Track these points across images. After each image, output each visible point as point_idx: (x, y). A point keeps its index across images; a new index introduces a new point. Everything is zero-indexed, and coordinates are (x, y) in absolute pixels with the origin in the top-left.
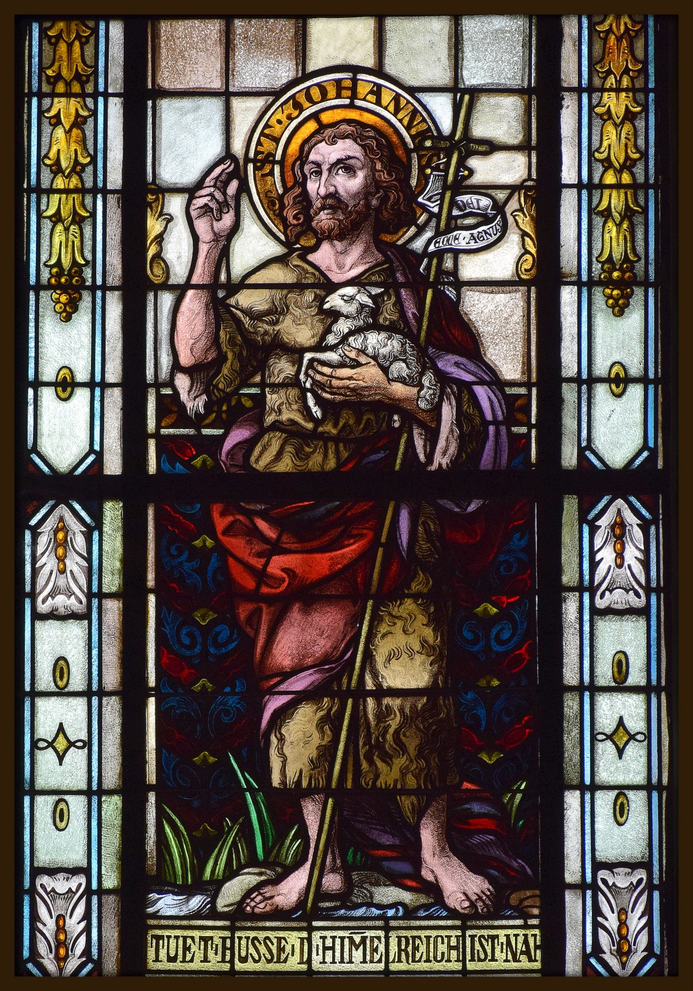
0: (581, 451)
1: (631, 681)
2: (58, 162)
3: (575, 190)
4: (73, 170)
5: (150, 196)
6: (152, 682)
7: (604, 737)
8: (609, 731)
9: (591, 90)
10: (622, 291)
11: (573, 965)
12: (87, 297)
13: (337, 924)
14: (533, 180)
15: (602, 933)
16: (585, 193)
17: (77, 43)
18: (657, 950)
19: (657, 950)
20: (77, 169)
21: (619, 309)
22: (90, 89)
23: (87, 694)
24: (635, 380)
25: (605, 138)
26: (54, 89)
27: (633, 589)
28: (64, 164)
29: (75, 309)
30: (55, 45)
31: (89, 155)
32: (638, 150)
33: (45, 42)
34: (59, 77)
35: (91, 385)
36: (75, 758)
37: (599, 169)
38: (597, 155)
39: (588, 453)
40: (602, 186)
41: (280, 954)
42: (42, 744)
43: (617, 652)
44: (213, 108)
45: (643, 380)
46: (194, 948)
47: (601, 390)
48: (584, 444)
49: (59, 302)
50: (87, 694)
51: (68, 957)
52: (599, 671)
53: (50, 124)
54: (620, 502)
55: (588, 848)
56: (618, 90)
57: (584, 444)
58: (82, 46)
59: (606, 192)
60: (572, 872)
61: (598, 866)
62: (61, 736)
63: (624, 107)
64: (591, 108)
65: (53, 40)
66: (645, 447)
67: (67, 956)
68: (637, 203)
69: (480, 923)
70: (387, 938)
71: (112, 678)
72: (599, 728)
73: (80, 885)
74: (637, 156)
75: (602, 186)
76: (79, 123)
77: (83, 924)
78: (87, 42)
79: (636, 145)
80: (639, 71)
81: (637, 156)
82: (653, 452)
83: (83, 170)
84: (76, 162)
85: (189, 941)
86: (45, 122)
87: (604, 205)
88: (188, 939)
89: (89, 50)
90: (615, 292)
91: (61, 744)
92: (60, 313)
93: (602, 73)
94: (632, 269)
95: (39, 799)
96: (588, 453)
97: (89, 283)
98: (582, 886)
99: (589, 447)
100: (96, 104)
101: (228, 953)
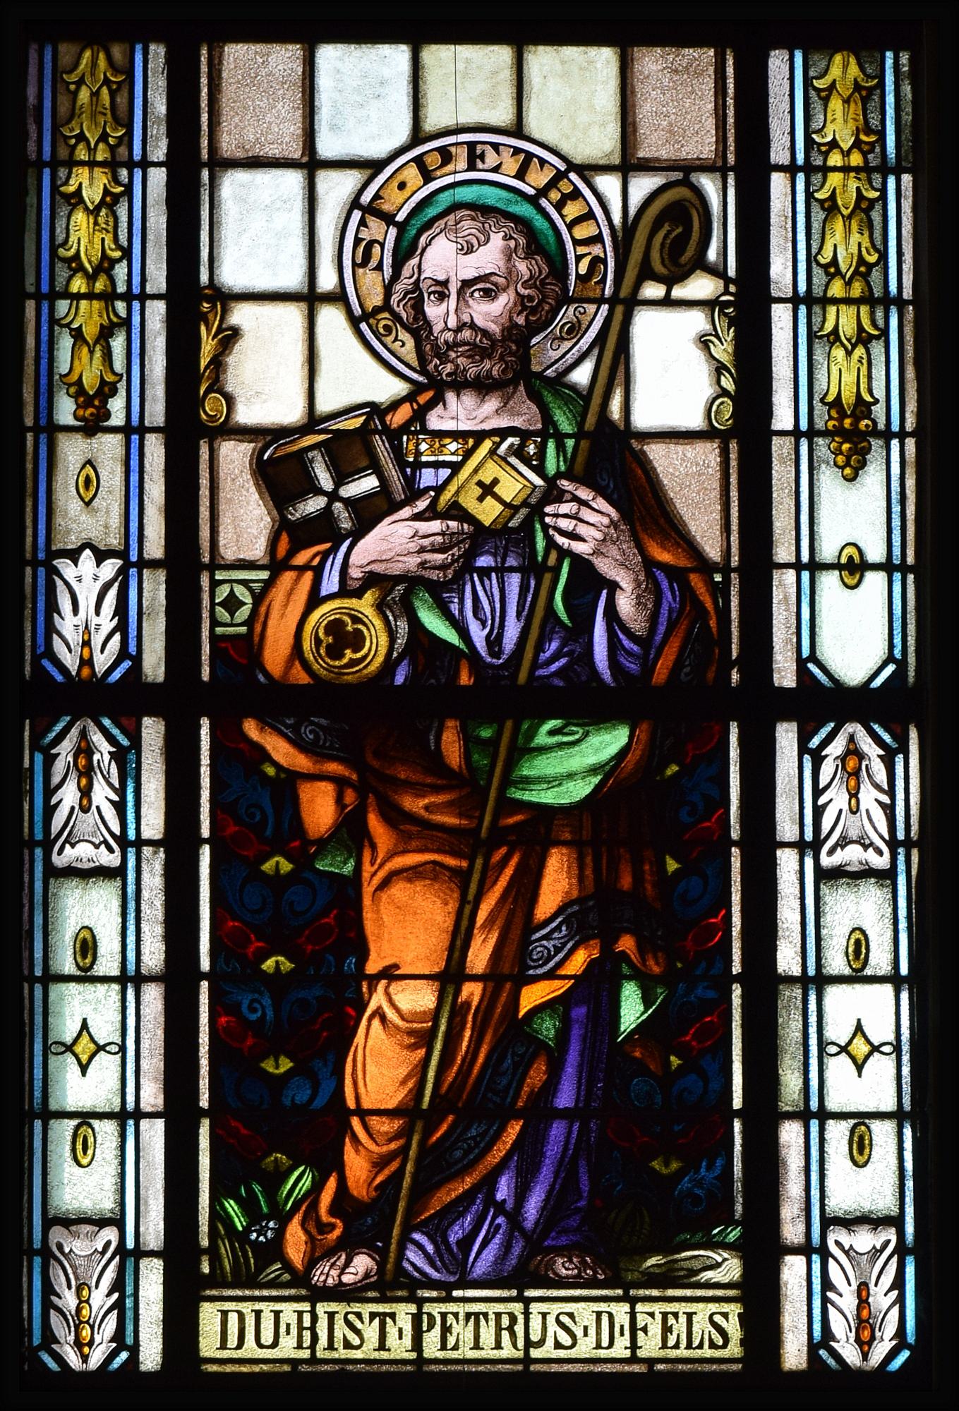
0: (801, 663)
1: (102, 968)
2: (834, 261)
3: (790, 306)
4: (856, 272)
5: (206, 305)
6: (205, 964)
7: (882, 1049)
8: (68, 1039)
9: (808, 169)
10: (855, 444)
11: (794, 1354)
12: (876, 444)
13: (699, 1293)
14: (731, 294)
15: (832, 1313)
16: (803, 310)
17: (105, 90)
18: (911, 1338)
19: (911, 1338)
20: (863, 270)
21: (853, 468)
22: (874, 160)
23: (122, 980)
24: (876, 567)
25: (828, 237)
26: (825, 160)
27: (105, 842)
28: (843, 268)
29: (863, 464)
30: (826, 101)
31: (877, 250)
32: (119, 247)
33: (813, 93)
34: (834, 144)
35: (815, 567)
36: (106, 1066)
37: (819, 277)
38: (61, 251)
39: (811, 666)
40: (826, 301)
41: (667, 1336)
42: (832, 1049)
43: (83, 928)
44: (293, 180)
45: (887, 567)
46: (457, 1329)
47: (829, 582)
48: (806, 652)
49: (841, 453)
50: (122, 980)
51: (875, 1339)
52: (145, 958)
53: (823, 208)
54: (850, 728)
55: (815, 1193)
56: (92, 164)
57: (806, 652)
58: (113, 94)
59: (832, 310)
60: (792, 1232)
61: (828, 1222)
62: (85, 1036)
63: (102, 187)
64: (809, 196)
65: (823, 94)
66: (890, 659)
67: (873, 1338)
68: (874, 323)
69: (471, 1293)
70: (527, 1314)
71: (154, 955)
72: (830, 1034)
73: (888, 1241)
74: (117, 254)
75: (826, 301)
76: (109, 201)
77: (895, 1293)
78: (119, 89)
79: (873, 245)
80: (120, 138)
81: (117, 254)
82: (902, 664)
83: (112, 267)
84: (861, 261)
85: (450, 1319)
86: (815, 208)
87: (829, 326)
88: (449, 1315)
89: (122, 100)
90: (846, 446)
91: (860, 1048)
92: (843, 468)
93: (824, 144)
94: (868, 415)
95: (831, 1124)
96: (811, 666)
97: (881, 426)
98: (805, 1250)
99: (813, 658)
100: (884, 184)
101: (307, 1335)
